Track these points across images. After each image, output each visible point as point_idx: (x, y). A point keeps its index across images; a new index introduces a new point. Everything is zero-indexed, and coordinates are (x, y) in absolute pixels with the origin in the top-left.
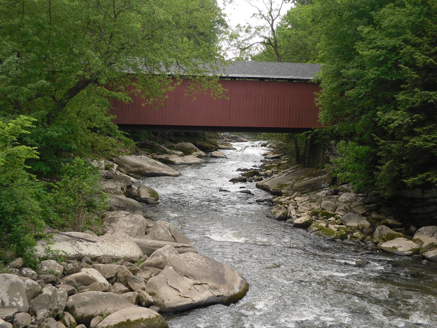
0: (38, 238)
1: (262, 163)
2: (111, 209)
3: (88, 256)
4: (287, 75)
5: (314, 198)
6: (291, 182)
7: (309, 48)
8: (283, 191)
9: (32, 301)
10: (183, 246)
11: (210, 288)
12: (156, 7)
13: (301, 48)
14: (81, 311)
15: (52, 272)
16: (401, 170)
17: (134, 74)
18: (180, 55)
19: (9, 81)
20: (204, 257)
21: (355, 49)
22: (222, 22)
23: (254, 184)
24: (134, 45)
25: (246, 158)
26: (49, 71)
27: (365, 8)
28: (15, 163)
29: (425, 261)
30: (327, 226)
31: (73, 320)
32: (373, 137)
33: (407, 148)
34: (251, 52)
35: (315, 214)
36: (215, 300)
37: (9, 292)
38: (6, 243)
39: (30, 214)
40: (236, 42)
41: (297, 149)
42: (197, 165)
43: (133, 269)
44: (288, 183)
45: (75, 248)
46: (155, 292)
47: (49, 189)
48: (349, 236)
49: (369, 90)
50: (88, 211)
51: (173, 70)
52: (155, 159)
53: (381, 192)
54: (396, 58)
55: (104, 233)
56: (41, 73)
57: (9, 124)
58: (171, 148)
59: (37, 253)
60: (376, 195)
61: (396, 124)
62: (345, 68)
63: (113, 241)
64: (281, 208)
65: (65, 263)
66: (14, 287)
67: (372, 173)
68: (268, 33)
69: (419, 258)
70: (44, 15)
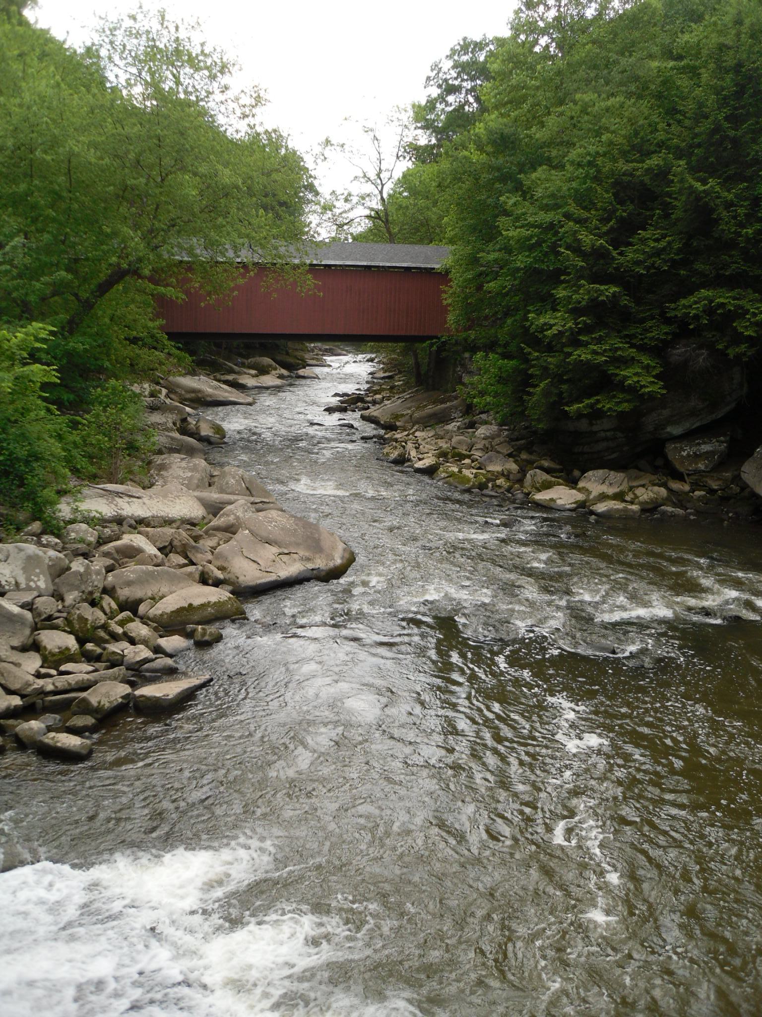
0: (61, 493)
1: (368, 386)
2: (160, 452)
3: (131, 518)
4: (404, 261)
5: (442, 433)
6: (409, 412)
7: (432, 224)
8: (398, 424)
9: (57, 580)
10: (261, 502)
11: (302, 559)
12: (220, 167)
13: (422, 225)
14: (124, 593)
15: (82, 541)
16: (561, 393)
17: (189, 262)
18: (254, 234)
19: (15, 272)
20: (292, 516)
21: (498, 226)
22: (311, 188)
23: (358, 414)
24: (189, 221)
25: (346, 378)
26: (69, 259)
27: (510, 168)
28: (26, 389)
29: (592, 518)
30: (460, 472)
31: (114, 606)
32: (523, 349)
33: (569, 363)
34: (352, 230)
35: (443, 454)
36: (308, 575)
37: (25, 569)
38: (17, 501)
39: (49, 460)
40: (330, 216)
41: (418, 365)
42: (278, 389)
43: (194, 534)
44: (405, 413)
45: (113, 506)
46: (225, 565)
47: (75, 425)
48: (490, 485)
49: (516, 282)
50: (129, 455)
51: (245, 256)
52: (219, 381)
53: (533, 423)
54: (554, 239)
55: (151, 485)
56: (58, 262)
57: (18, 334)
58: (243, 365)
59: (60, 514)
60: (526, 428)
61: (554, 330)
62: (484, 251)
63: (165, 496)
64: (396, 448)
65: (100, 528)
66: (31, 562)
67: (521, 398)
68: (376, 204)
69: (586, 513)
70: (62, 179)
